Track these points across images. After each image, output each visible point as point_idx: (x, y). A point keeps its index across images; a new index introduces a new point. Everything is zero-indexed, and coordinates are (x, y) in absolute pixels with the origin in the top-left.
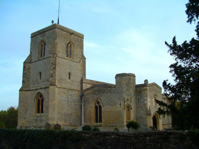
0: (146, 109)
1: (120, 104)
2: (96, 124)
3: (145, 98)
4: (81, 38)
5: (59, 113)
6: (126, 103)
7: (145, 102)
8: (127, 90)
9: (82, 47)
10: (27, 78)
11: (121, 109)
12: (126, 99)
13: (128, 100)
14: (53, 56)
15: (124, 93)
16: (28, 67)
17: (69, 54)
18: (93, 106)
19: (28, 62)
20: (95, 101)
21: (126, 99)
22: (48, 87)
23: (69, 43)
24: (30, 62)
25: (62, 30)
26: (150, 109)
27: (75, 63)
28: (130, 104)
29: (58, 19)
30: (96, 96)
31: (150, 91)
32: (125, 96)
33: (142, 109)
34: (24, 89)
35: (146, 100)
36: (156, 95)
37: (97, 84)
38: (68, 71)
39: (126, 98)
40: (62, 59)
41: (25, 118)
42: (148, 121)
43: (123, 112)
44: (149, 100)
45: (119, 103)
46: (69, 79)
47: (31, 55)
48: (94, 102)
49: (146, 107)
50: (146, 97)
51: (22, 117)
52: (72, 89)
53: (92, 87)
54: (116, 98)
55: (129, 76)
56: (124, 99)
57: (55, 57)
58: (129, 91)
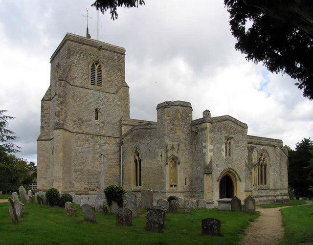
0: (205, 163)
1: (161, 156)
2: (136, 187)
3: (204, 144)
4: (120, 53)
5: (76, 171)
6: (169, 155)
7: (204, 151)
8: (171, 130)
9: (121, 69)
10: (46, 123)
11: (163, 164)
12: (169, 147)
13: (173, 148)
14: (61, 84)
15: (166, 137)
16: (47, 106)
17: (96, 79)
18: (132, 159)
19: (48, 99)
20: (134, 151)
21: (169, 147)
22: (275, 147)
23: (97, 64)
24: (50, 99)
25: (80, 43)
26: (211, 163)
27: (108, 94)
28: (176, 155)
29: (87, 29)
30: (135, 144)
31: (212, 131)
32: (167, 141)
33: (200, 164)
34: (44, 138)
35: (205, 147)
36: (232, 138)
37: (137, 124)
38: (93, 107)
39: (169, 144)
40: (81, 89)
41: (46, 178)
42: (205, 185)
43: (164, 170)
44: (210, 147)
45: (160, 154)
46: (97, 118)
47: (60, 90)
48: (133, 154)
49: (205, 159)
50: (206, 141)
51: (42, 177)
52: (102, 134)
53: (131, 131)
54: (157, 146)
55: (175, 105)
56: (167, 146)
57: (62, 85)
58: (175, 133)
